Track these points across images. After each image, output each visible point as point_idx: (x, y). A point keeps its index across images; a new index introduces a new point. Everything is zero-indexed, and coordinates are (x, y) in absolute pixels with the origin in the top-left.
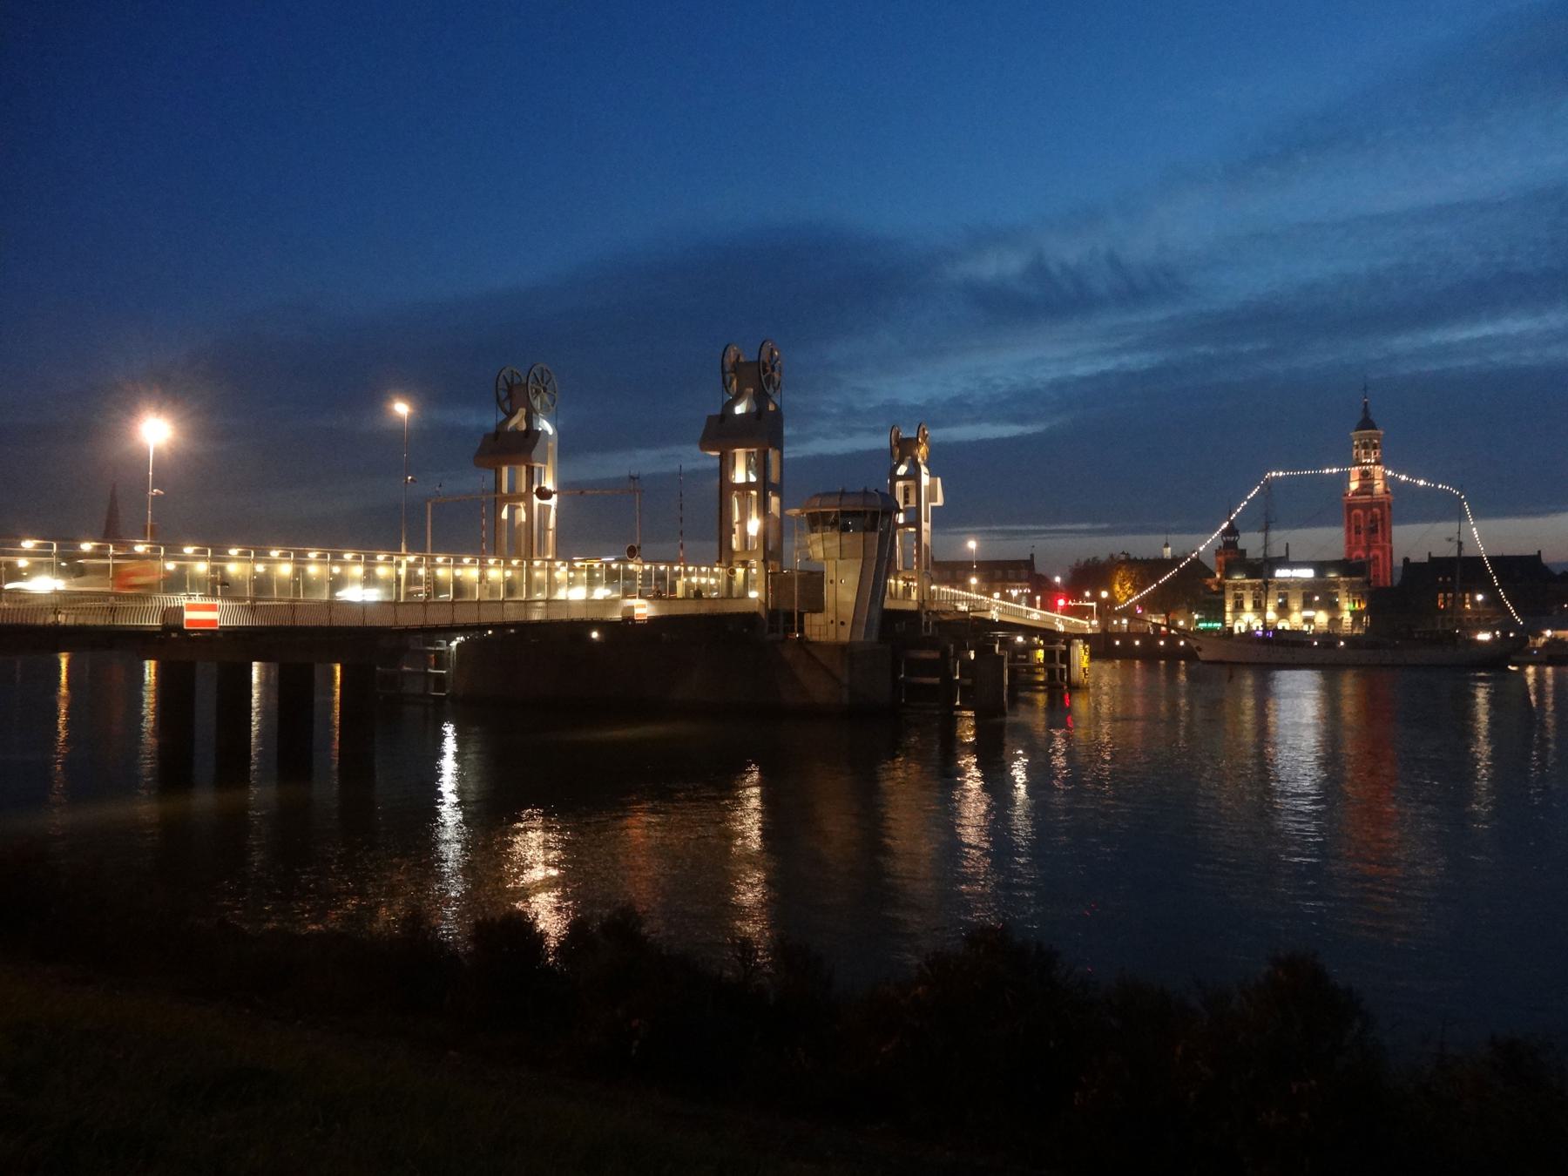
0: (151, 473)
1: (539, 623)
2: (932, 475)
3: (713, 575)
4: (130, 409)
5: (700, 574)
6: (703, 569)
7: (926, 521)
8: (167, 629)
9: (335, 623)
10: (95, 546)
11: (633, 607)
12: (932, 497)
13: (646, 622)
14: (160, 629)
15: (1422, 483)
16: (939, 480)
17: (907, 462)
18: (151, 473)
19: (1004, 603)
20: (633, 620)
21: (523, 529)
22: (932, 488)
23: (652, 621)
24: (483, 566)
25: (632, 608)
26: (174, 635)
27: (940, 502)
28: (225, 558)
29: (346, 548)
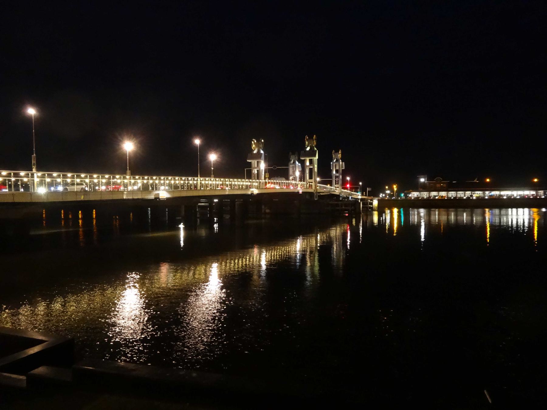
0: (128, 158)
1: (125, 200)
2: (342, 162)
3: (221, 181)
4: (349, 177)
5: (238, 181)
6: (239, 180)
7: (316, 164)
8: (156, 198)
9: (103, 199)
10: (57, 175)
11: (253, 191)
12: (342, 167)
13: (165, 199)
14: (154, 198)
15: (247, 352)
16: (344, 163)
17: (309, 146)
18: (128, 158)
19: (173, 187)
20: (159, 198)
21: (256, 174)
22: (342, 164)
23: (258, 194)
24: (91, 177)
25: (158, 194)
26: (158, 200)
27: (344, 168)
28: (41, 178)
29: (153, 176)
